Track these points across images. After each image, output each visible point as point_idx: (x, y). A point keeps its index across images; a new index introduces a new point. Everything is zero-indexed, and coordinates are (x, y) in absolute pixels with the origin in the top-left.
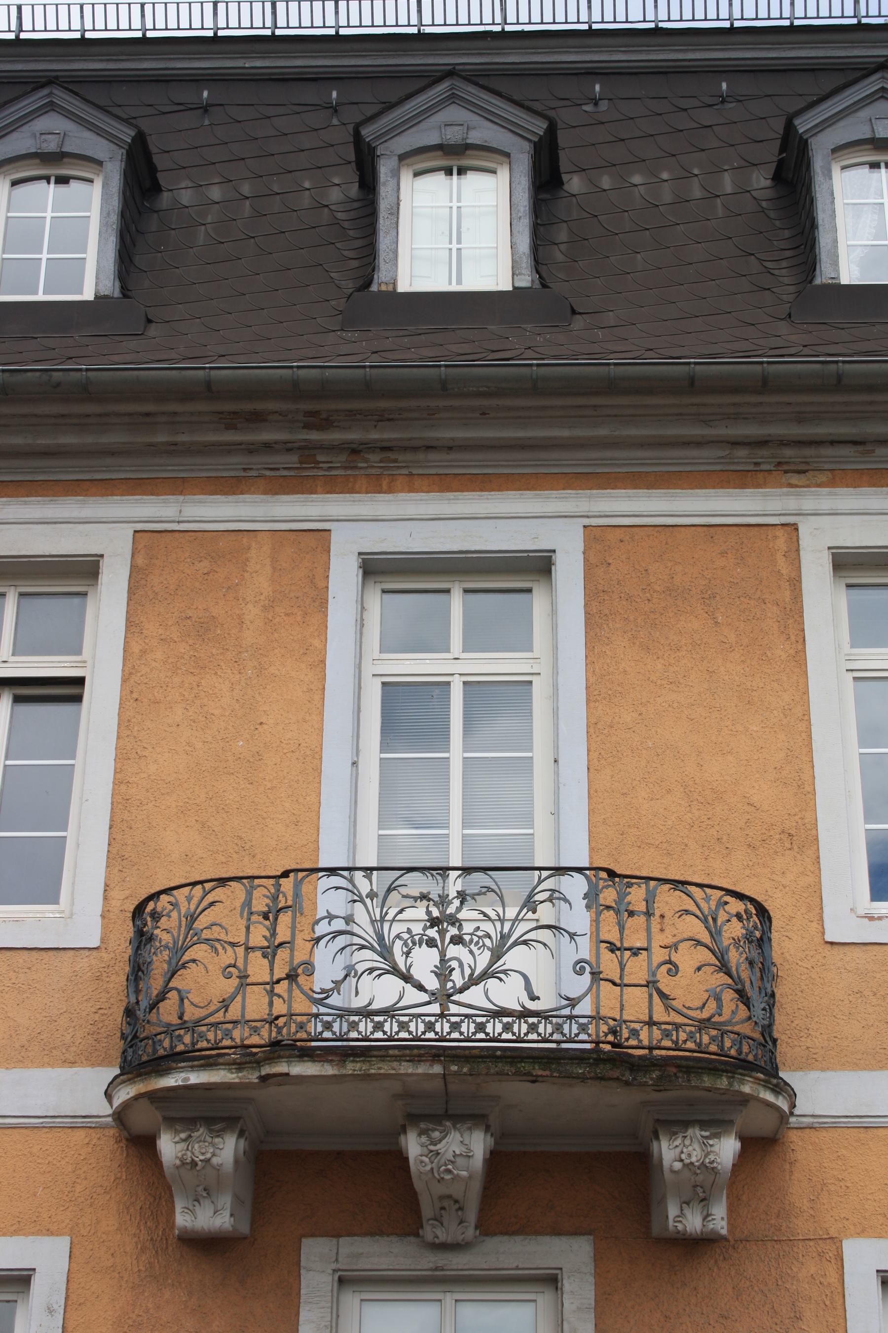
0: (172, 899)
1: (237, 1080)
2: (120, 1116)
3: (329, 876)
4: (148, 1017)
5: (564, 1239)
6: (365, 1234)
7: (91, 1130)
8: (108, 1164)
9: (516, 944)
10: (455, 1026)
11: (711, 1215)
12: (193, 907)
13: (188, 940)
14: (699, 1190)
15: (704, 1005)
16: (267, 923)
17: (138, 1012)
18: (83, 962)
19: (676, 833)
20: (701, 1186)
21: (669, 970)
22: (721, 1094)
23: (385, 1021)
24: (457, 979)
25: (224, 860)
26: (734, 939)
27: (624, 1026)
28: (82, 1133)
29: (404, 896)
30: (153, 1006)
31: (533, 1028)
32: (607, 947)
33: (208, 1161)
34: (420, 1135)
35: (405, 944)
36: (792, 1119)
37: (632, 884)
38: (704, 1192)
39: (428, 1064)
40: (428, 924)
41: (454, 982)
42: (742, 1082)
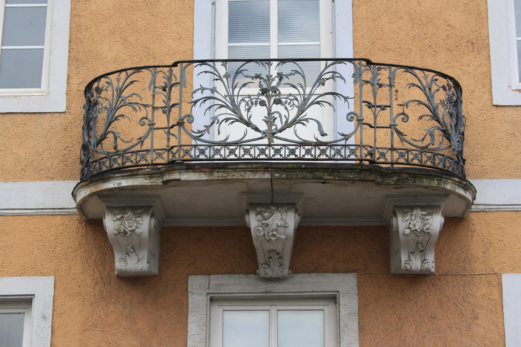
0: (107, 80)
1: (150, 184)
2: (81, 207)
3: (201, 65)
4: (96, 149)
5: (340, 275)
6: (225, 273)
7: (65, 216)
8: (75, 235)
9: (313, 103)
10: (277, 151)
11: (426, 260)
12: (121, 84)
13: (119, 103)
14: (420, 245)
15: (424, 138)
16: (165, 93)
17: (90, 146)
18: (57, 121)
19: (405, 43)
20: (420, 243)
21: (404, 118)
22: (433, 190)
23: (236, 149)
24: (279, 124)
25: (138, 61)
26: (441, 101)
27: (376, 151)
28: (59, 218)
29: (246, 77)
30: (99, 142)
31: (323, 152)
32: (366, 105)
33: (133, 231)
34: (257, 215)
35: (247, 104)
36: (473, 207)
37: (381, 69)
38: (422, 247)
39: (262, 173)
40: (261, 92)
41: (276, 126)
42: (446, 183)
